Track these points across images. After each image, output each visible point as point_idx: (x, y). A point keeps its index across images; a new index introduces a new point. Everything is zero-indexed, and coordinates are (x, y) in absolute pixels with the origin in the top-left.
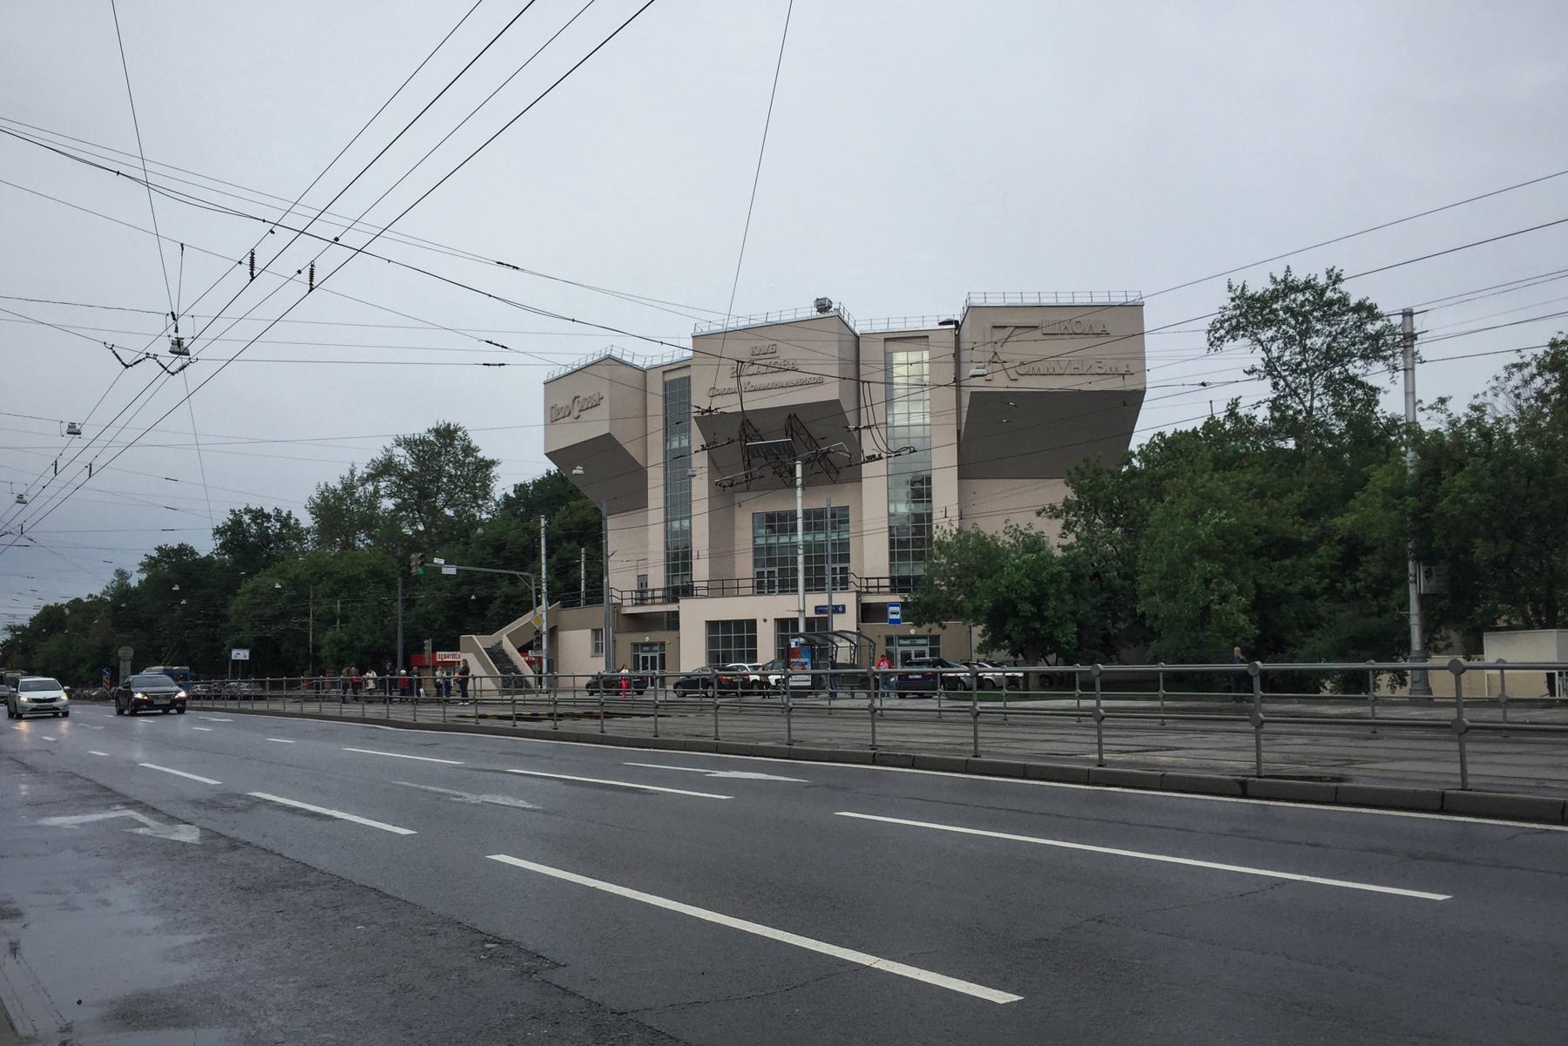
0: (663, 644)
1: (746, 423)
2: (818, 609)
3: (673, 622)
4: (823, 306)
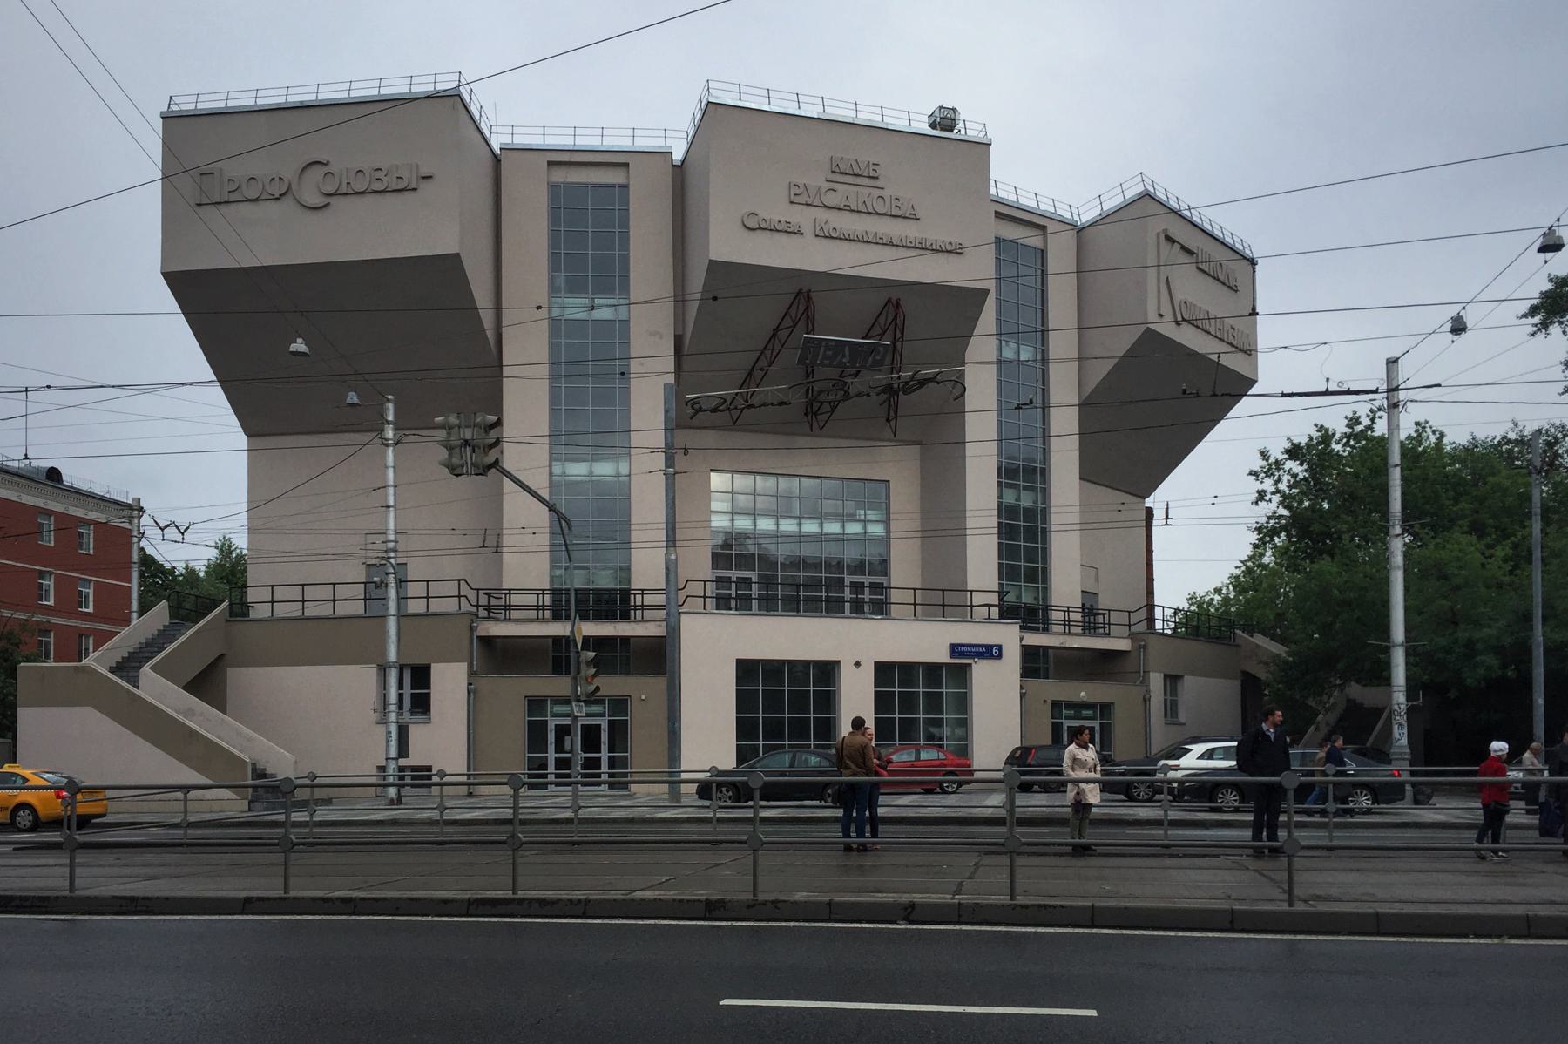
0: (1105, 709)
1: (802, 295)
2: (954, 649)
4: (945, 121)
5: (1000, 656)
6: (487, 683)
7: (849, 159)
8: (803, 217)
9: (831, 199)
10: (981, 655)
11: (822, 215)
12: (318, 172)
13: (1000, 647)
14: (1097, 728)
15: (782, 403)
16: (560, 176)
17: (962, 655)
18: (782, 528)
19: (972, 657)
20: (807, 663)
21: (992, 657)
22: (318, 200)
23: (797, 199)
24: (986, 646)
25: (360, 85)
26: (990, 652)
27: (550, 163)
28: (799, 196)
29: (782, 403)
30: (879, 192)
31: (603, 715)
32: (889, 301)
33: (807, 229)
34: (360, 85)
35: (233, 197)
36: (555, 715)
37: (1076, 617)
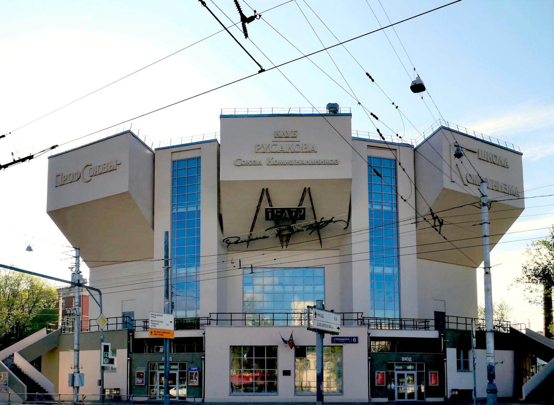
3: (197, 345)
4: (333, 109)
5: (357, 342)
6: (135, 356)
7: (282, 130)
8: (262, 158)
9: (275, 149)
10: (347, 342)
11: (271, 155)
12: (88, 168)
13: (357, 338)
14: (416, 374)
15: (264, 237)
16: (176, 157)
17: (337, 342)
18: (295, 290)
19: (343, 343)
20: (263, 347)
21: (353, 342)
22: (88, 179)
23: (259, 151)
24: (350, 338)
25: (362, 133)
26: (352, 340)
27: (172, 153)
28: (260, 149)
29: (264, 237)
30: (297, 143)
31: (177, 370)
32: (263, 189)
33: (264, 162)
34: (362, 133)
35: (66, 182)
36: (397, 370)
37: (432, 323)
